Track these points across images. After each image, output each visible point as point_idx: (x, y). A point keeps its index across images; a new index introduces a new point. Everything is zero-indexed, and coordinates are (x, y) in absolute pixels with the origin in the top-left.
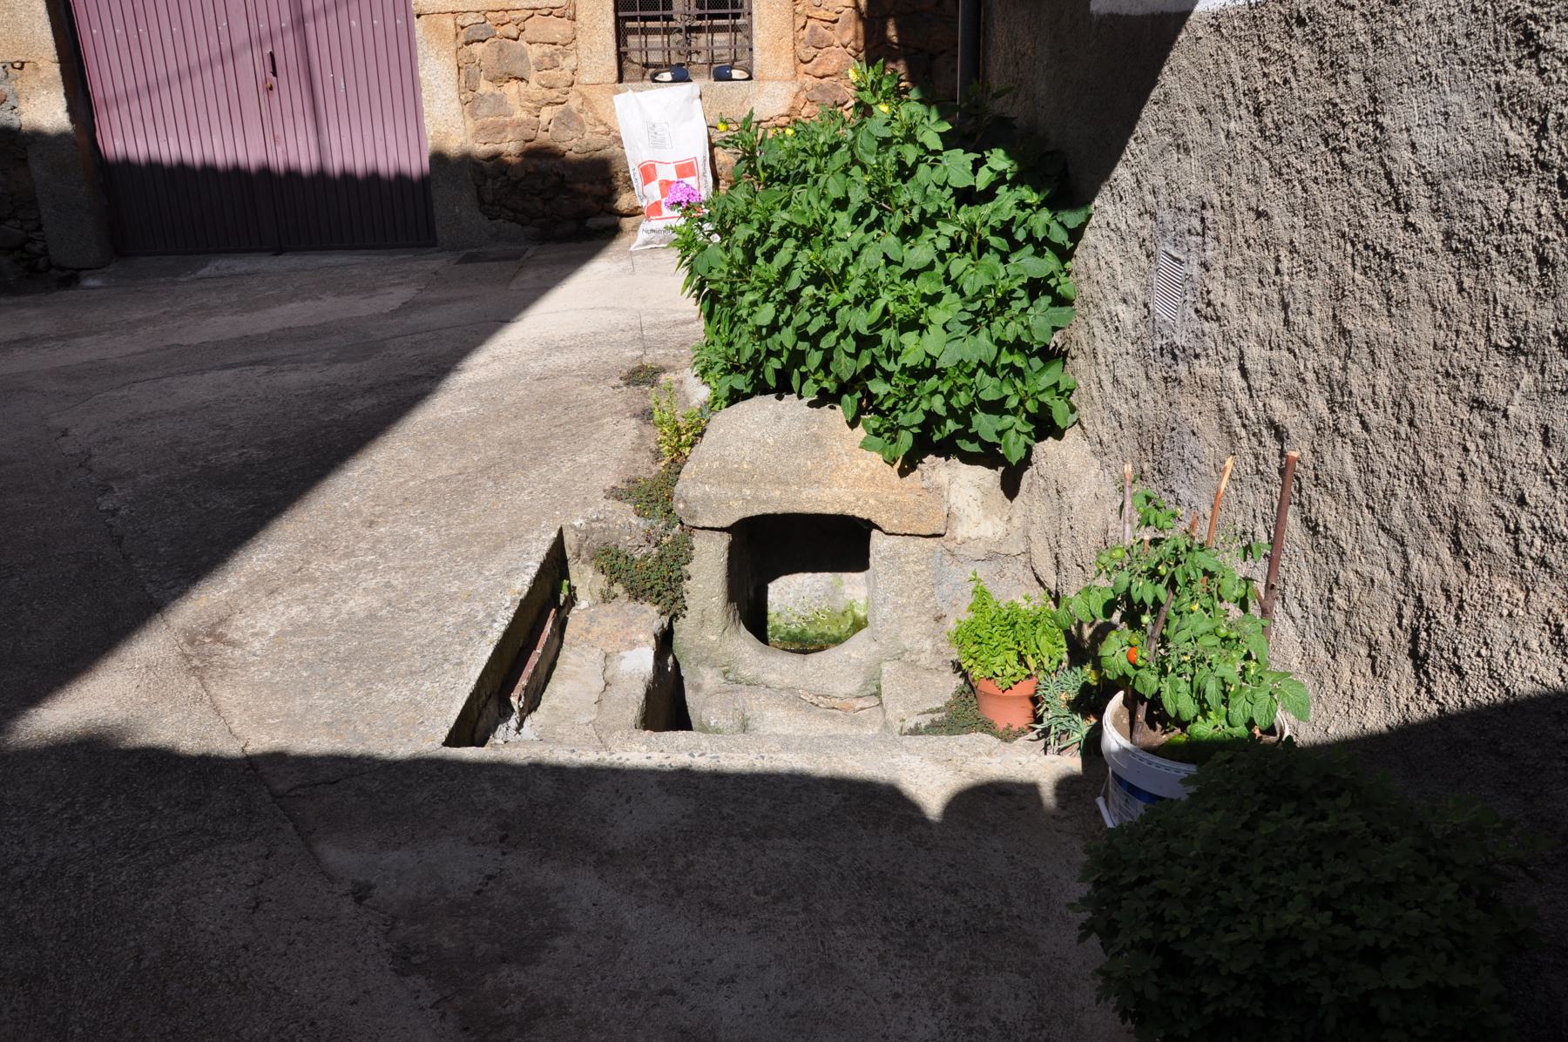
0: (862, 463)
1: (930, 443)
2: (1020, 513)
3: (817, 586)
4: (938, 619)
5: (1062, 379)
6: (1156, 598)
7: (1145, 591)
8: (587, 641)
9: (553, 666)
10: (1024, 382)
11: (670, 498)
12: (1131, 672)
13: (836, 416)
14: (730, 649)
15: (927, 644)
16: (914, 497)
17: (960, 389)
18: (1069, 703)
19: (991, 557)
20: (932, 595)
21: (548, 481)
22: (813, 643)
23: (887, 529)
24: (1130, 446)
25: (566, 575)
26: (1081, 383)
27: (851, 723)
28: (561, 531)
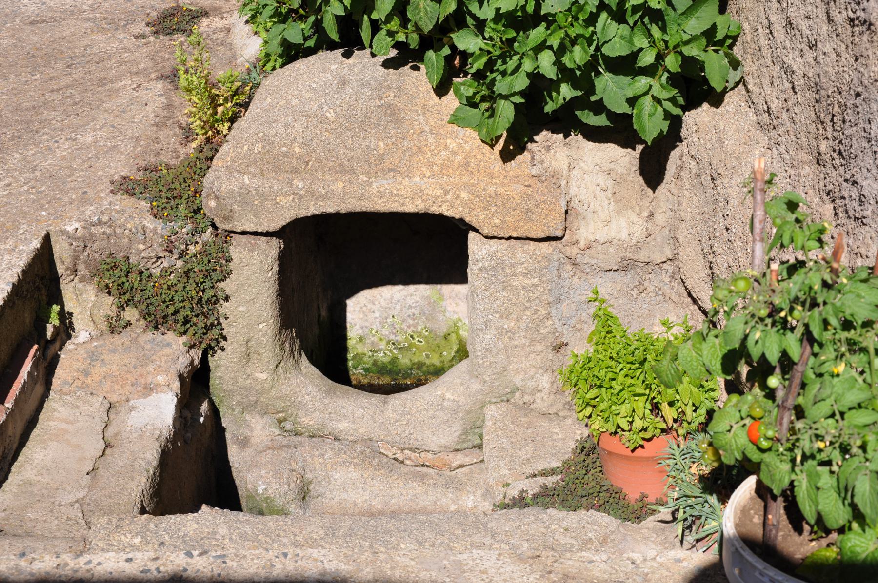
0: (452, 144)
1: (534, 118)
2: (664, 206)
3: (409, 301)
4: (558, 348)
5: (720, 20)
6: (785, 354)
7: (768, 344)
8: (84, 386)
9: (32, 423)
10: (664, 29)
11: (197, 192)
12: (755, 456)
13: (418, 81)
14: (286, 390)
15: (545, 381)
16: (520, 188)
17: (573, 42)
18: (702, 478)
19: (625, 266)
20: (548, 316)
21: (34, 169)
22: (407, 376)
23: (485, 231)
24: (805, 115)
25: (56, 297)
26: (746, 26)
27: (447, 486)
28: (47, 239)
